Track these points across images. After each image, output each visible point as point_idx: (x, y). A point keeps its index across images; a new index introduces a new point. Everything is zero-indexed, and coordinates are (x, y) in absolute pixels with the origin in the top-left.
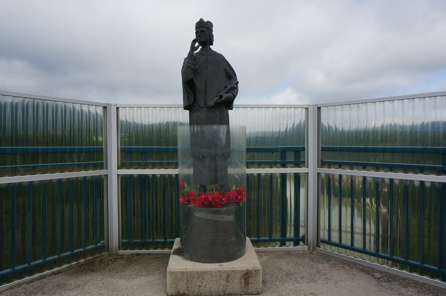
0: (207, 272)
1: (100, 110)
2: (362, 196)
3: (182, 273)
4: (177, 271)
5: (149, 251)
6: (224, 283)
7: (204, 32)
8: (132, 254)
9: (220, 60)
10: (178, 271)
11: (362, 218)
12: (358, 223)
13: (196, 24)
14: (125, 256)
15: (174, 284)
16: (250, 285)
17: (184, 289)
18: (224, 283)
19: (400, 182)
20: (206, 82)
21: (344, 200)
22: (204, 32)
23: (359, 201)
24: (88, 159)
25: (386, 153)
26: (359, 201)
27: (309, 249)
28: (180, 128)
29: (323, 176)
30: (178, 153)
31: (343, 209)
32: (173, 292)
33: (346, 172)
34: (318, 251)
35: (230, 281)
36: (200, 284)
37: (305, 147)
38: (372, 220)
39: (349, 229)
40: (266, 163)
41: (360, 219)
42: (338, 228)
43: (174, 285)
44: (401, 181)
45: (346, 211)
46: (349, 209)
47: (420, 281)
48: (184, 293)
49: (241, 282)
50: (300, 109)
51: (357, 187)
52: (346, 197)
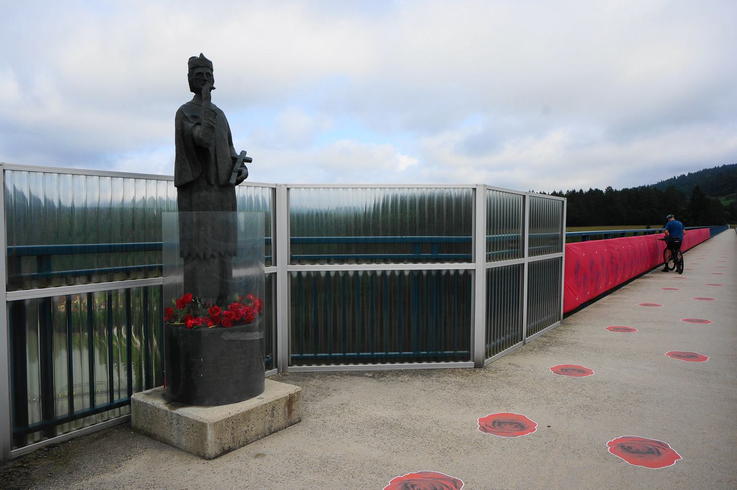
0: (252, 410)
1: (268, 194)
2: (105, 324)
3: (227, 420)
4: (220, 419)
5: (71, 434)
6: (270, 419)
7: (200, 73)
8: (40, 449)
9: (217, 115)
10: (222, 419)
11: (106, 363)
12: (101, 372)
13: (211, 63)
14: (31, 456)
15: (218, 439)
16: (293, 412)
17: (229, 442)
18: (270, 419)
19: (410, 273)
20: (215, 148)
21: (76, 337)
22: (200, 73)
23: (101, 334)
24: (495, 249)
25: (77, 255)
26: (101, 334)
27: (278, 372)
28: (165, 215)
29: (295, 275)
30: (179, 253)
31: (76, 354)
32: (217, 451)
33: (79, 289)
34: (289, 371)
35: (275, 413)
36: (246, 428)
37: (471, 238)
38: (121, 365)
39: (87, 389)
40: (101, 273)
41: (104, 366)
42: (66, 393)
43: (218, 441)
44: (411, 272)
45: (81, 359)
46: (86, 353)
47: (402, 369)
48: (229, 447)
49: (285, 412)
50: (70, 176)
51: (97, 310)
52: (79, 332)
